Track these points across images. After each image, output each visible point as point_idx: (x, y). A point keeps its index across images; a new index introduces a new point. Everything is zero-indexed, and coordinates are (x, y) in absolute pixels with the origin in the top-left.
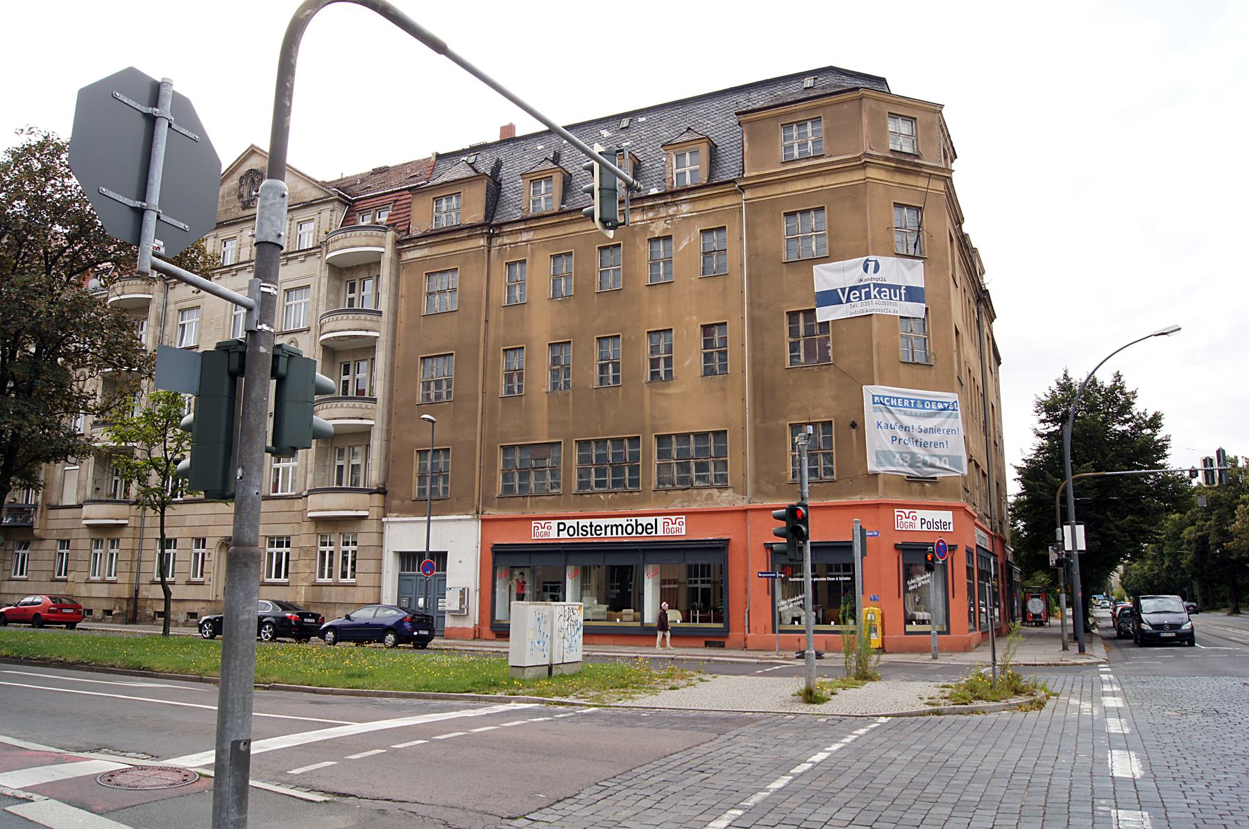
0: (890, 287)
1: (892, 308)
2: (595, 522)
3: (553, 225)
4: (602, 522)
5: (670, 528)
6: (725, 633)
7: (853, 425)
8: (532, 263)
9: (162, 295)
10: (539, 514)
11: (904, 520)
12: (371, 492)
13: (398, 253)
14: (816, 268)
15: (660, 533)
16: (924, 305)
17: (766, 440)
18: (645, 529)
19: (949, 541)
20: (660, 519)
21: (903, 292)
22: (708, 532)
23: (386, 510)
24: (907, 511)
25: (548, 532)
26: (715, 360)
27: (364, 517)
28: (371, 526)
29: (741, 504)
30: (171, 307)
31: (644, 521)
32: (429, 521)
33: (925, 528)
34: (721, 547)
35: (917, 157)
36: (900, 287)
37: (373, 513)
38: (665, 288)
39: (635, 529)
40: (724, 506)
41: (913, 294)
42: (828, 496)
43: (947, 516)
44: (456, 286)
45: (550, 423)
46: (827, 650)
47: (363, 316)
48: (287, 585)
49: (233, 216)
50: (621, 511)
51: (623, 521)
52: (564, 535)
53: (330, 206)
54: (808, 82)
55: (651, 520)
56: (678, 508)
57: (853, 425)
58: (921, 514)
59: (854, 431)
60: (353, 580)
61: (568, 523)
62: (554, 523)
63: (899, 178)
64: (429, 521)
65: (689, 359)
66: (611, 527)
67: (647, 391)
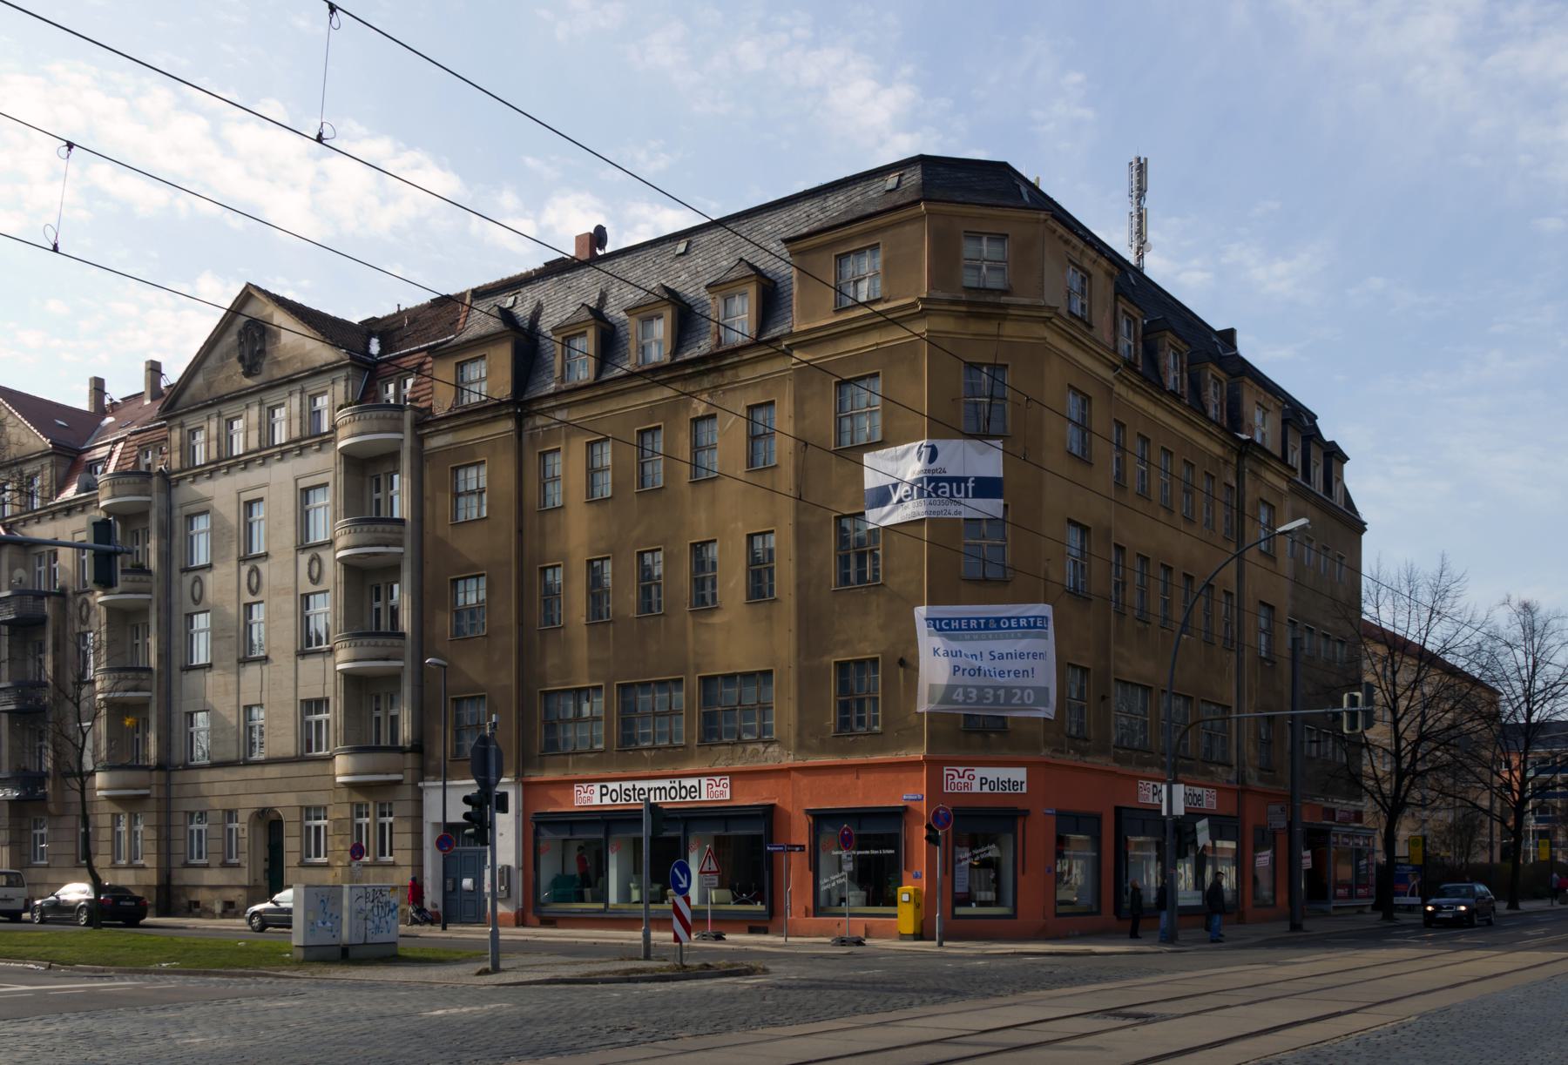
0: (950, 480)
1: (953, 508)
2: (639, 784)
3: (587, 401)
4: (645, 785)
5: (713, 791)
6: (773, 912)
7: (902, 662)
8: (567, 454)
9: (163, 496)
10: (581, 774)
11: (957, 780)
12: (402, 750)
13: (419, 440)
14: (868, 458)
15: (704, 798)
16: (1001, 501)
17: (808, 680)
18: (689, 792)
19: (1021, 806)
20: (704, 781)
21: (970, 485)
22: (752, 797)
23: (422, 772)
24: (961, 769)
25: (590, 797)
26: (759, 584)
27: (398, 783)
28: (407, 793)
29: (789, 761)
30: (177, 512)
31: (688, 783)
32: (445, 787)
33: (986, 789)
34: (768, 814)
35: (1005, 292)
36: (965, 480)
37: (407, 777)
38: (708, 486)
39: (678, 793)
40: (770, 764)
41: (986, 487)
42: (873, 751)
43: (1019, 774)
44: (483, 483)
45: (591, 662)
46: (867, 936)
47: (380, 527)
48: (327, 865)
49: (236, 387)
50: (668, 770)
51: (666, 784)
52: (607, 800)
53: (343, 374)
54: (892, 181)
55: (694, 782)
56: (719, 767)
57: (902, 662)
58: (980, 772)
59: (901, 670)
60: (391, 859)
61: (612, 786)
62: (597, 787)
63: (975, 327)
64: (445, 787)
65: (732, 581)
66: (659, 790)
67: (690, 620)
